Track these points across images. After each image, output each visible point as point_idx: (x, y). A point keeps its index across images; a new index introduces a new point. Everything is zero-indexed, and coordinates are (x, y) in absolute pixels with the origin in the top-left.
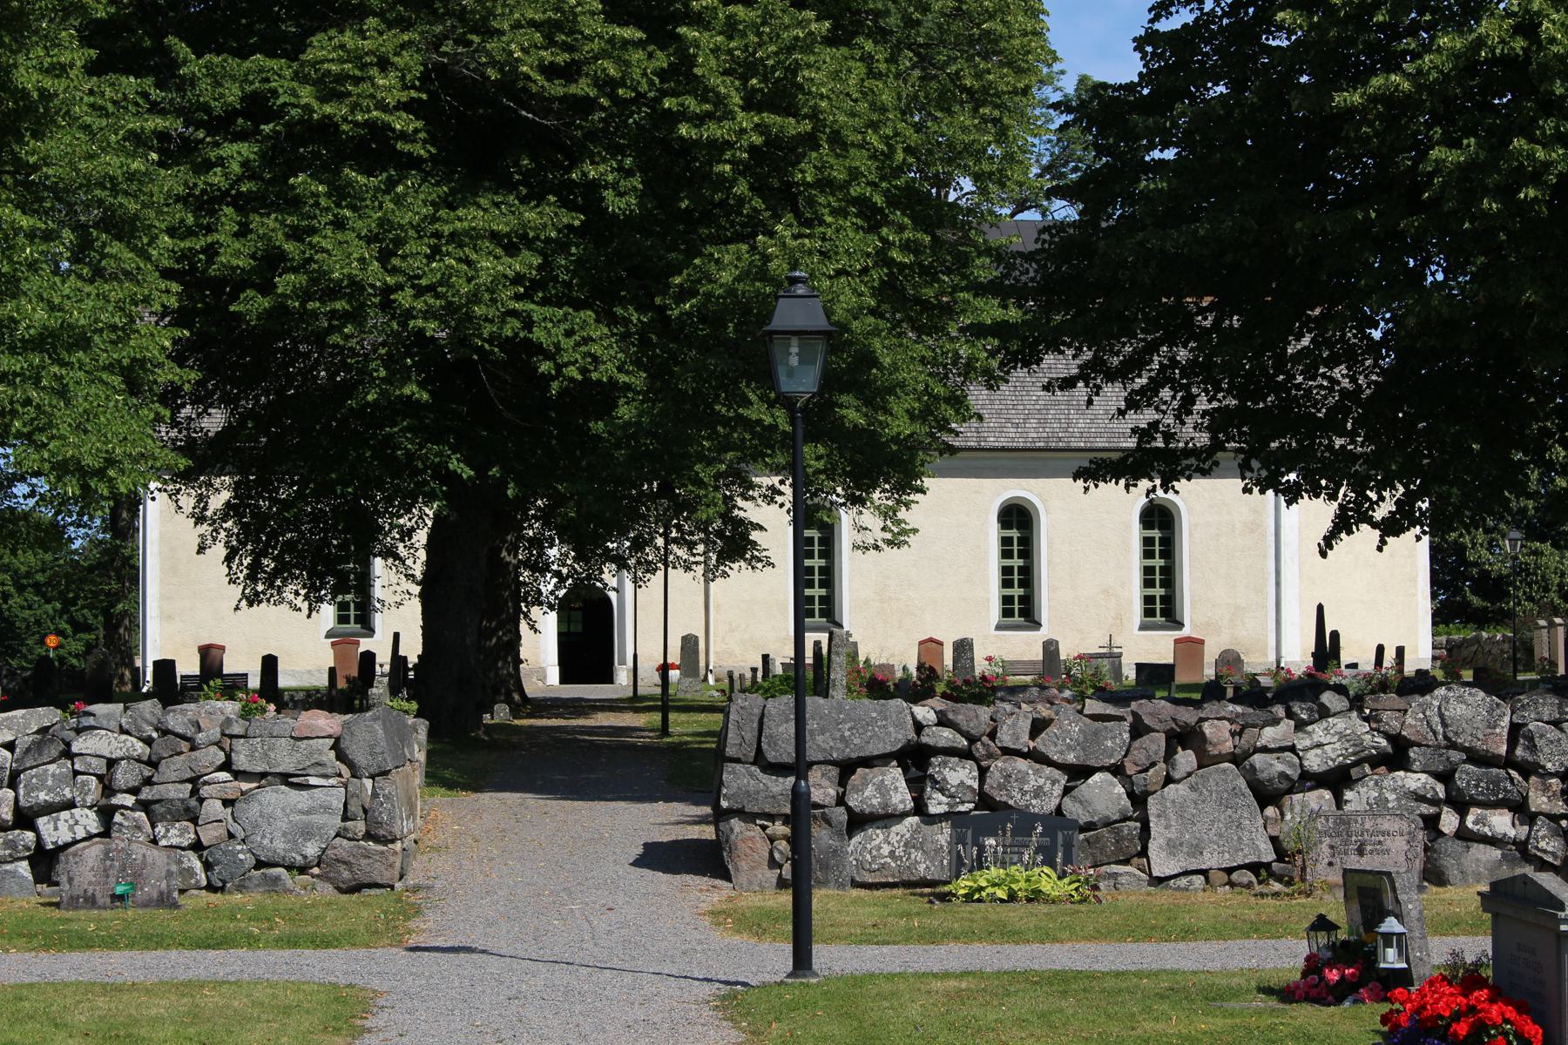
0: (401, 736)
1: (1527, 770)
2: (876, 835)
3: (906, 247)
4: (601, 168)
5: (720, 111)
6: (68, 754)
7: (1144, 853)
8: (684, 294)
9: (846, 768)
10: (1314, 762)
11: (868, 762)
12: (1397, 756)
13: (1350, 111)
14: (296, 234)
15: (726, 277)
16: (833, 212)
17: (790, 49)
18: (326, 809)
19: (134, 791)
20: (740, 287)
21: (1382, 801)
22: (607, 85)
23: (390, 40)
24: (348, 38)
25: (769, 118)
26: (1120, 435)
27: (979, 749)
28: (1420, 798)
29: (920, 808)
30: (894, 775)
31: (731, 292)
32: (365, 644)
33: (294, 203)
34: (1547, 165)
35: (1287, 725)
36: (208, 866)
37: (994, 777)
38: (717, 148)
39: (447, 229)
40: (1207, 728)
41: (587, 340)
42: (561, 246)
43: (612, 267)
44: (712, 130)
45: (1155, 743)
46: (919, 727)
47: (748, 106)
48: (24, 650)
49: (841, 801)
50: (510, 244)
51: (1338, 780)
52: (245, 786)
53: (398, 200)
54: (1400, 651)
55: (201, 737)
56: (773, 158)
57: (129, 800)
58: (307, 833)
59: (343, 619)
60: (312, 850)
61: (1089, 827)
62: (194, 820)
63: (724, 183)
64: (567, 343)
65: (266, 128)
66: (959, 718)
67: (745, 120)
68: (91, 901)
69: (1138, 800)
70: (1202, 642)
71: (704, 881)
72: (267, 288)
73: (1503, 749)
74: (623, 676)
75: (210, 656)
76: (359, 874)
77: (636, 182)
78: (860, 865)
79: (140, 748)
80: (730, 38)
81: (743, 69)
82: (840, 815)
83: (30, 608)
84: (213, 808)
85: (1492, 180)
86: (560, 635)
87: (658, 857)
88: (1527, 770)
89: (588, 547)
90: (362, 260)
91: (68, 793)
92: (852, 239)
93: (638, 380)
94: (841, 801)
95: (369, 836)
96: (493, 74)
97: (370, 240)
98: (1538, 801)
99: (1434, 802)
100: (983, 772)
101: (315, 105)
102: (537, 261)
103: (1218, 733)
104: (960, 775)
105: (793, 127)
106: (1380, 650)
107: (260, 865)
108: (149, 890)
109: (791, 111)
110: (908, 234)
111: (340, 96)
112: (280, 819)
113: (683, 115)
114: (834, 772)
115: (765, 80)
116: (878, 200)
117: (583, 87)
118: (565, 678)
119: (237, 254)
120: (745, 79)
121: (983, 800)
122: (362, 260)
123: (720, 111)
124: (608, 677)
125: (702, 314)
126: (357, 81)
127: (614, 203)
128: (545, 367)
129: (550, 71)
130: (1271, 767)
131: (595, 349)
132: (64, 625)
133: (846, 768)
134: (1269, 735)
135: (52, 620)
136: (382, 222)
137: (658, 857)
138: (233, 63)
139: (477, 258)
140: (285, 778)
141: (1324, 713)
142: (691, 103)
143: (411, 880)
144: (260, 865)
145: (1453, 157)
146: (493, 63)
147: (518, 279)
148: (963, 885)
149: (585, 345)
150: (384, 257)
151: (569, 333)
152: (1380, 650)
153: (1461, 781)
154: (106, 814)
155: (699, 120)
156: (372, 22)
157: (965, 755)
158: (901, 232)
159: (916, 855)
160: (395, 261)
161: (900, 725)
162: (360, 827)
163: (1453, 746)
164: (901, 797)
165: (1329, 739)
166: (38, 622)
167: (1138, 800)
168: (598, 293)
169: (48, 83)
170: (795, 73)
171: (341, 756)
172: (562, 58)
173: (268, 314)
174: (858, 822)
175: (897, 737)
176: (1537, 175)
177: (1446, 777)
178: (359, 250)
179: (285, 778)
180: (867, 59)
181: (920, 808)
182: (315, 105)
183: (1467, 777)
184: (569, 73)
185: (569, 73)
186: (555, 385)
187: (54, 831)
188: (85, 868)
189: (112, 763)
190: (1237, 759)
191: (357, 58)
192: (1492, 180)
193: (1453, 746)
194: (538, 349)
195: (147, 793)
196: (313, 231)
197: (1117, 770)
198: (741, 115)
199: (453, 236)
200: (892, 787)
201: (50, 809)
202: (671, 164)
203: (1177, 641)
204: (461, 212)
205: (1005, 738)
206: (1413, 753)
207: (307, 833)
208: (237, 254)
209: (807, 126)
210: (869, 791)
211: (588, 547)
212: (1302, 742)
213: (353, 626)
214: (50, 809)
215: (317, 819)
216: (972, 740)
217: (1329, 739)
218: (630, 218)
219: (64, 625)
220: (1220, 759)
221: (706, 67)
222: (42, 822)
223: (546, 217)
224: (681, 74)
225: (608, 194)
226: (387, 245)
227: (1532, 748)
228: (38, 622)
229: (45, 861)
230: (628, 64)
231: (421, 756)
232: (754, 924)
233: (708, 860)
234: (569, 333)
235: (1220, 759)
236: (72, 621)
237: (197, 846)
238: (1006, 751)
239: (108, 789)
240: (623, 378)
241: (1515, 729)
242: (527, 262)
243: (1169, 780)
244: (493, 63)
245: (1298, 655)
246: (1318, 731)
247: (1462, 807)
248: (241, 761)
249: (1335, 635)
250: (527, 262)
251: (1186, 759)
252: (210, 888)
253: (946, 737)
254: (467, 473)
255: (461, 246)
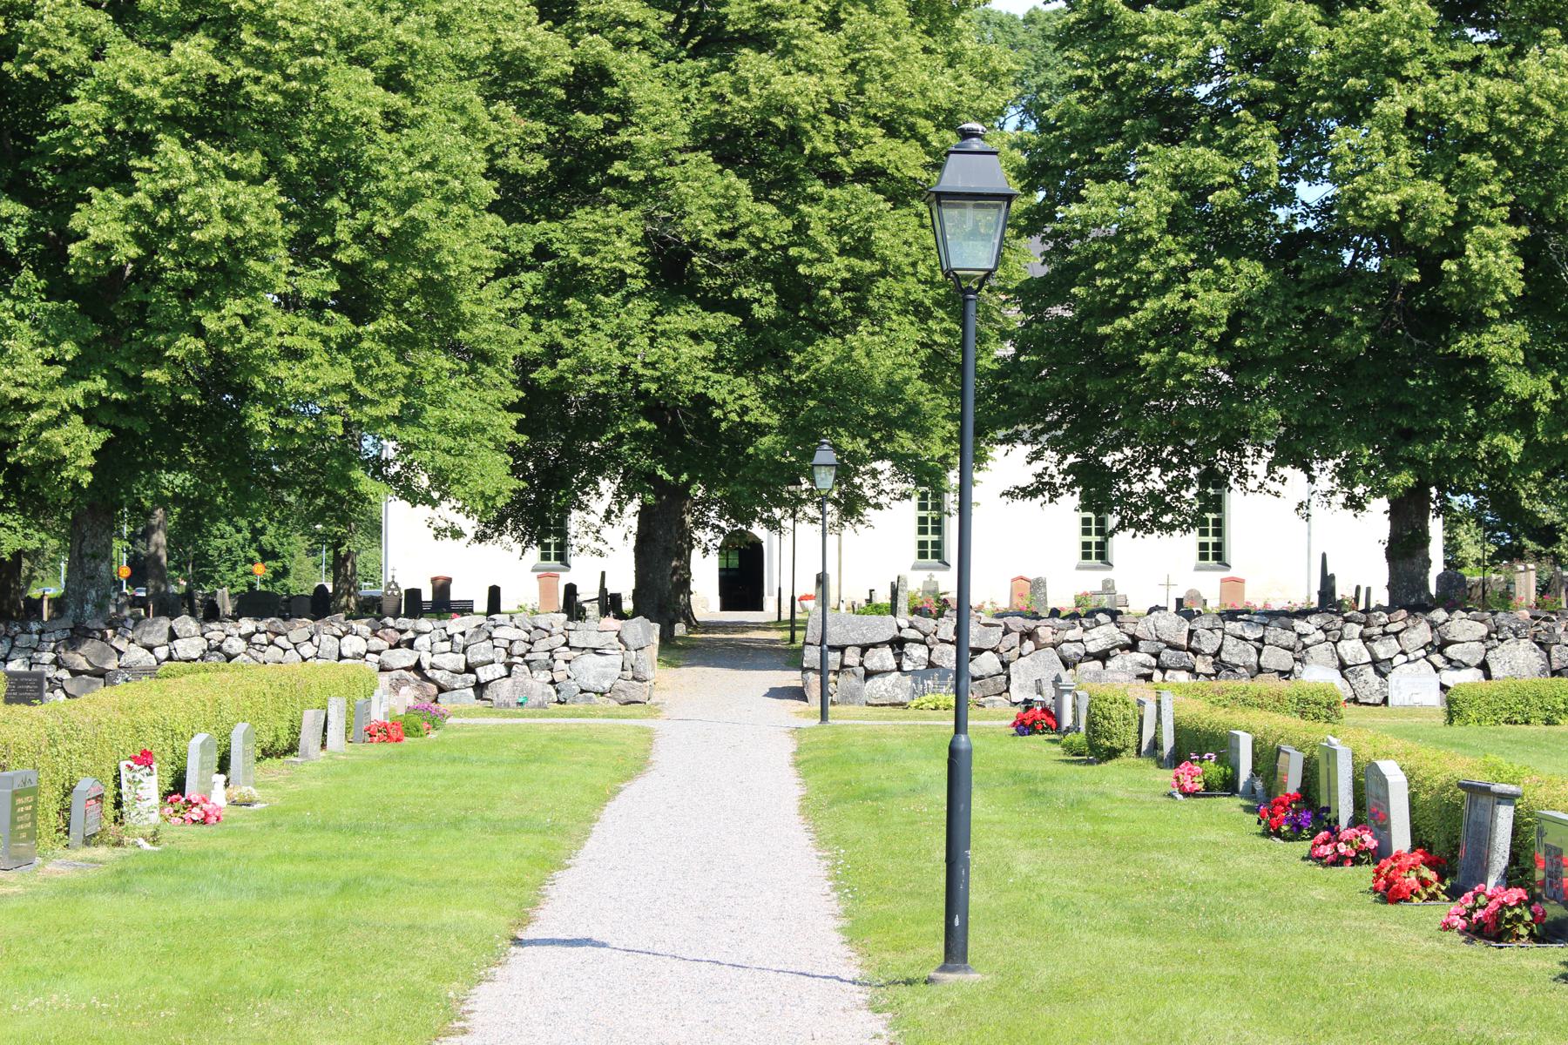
0: (648, 632)
1: (1196, 652)
2: (877, 680)
3: (947, 332)
4: (751, 290)
5: (824, 257)
6: (490, 638)
7: (1007, 690)
8: (800, 369)
9: (864, 649)
10: (1092, 648)
11: (874, 646)
12: (1133, 645)
13: (1107, 337)
14: (569, 334)
15: (827, 360)
16: (898, 313)
17: (867, 220)
18: (614, 665)
19: (522, 656)
20: (838, 367)
21: (1124, 667)
22: (755, 242)
23: (623, 218)
24: (598, 216)
25: (854, 261)
26: (1026, 478)
27: (929, 640)
28: (1144, 666)
29: (899, 668)
30: (887, 652)
31: (831, 370)
32: (565, 578)
33: (565, 315)
34: (1195, 365)
35: (1079, 629)
36: (558, 691)
37: (935, 654)
38: (822, 281)
39: (659, 328)
40: (1039, 630)
41: (742, 397)
42: (729, 335)
43: (759, 351)
44: (820, 270)
45: (1014, 638)
46: (900, 629)
47: (842, 252)
48: (217, 576)
49: (861, 664)
50: (695, 337)
51: (1103, 656)
52: (575, 653)
53: (629, 313)
54: (1368, 590)
55: (554, 631)
56: (857, 286)
57: (520, 660)
58: (605, 676)
59: (545, 557)
60: (607, 685)
61: (981, 678)
62: (551, 670)
63: (826, 302)
64: (730, 399)
65: (547, 264)
66: (919, 625)
67: (840, 262)
68: (507, 705)
69: (1005, 665)
70: (1242, 581)
71: (796, 702)
72: (553, 365)
73: (1184, 642)
74: (770, 602)
75: (442, 587)
76: (628, 696)
77: (773, 298)
78: (870, 695)
79: (526, 636)
80: (831, 210)
81: (836, 230)
82: (861, 671)
83: (222, 537)
84: (560, 664)
85: (1171, 370)
86: (721, 570)
87: (776, 693)
88: (1196, 652)
89: (739, 510)
90: (609, 350)
91: (491, 657)
92: (908, 331)
93: (774, 420)
94: (861, 664)
95: (634, 678)
96: (686, 238)
97: (614, 337)
98: (1200, 668)
99: (1150, 667)
100: (930, 651)
101: (579, 257)
102: (715, 347)
103: (1045, 633)
104: (918, 652)
105: (868, 267)
106: (1358, 588)
107: (582, 691)
108: (534, 701)
109: (871, 256)
110: (945, 325)
111: (592, 253)
112: (591, 670)
113: (800, 260)
114: (858, 650)
115: (852, 236)
116: (928, 302)
117: (740, 243)
118: (726, 606)
119: (534, 344)
120: (840, 237)
121: (931, 665)
122: (609, 350)
123: (824, 257)
124: (758, 605)
125: (813, 379)
126: (605, 244)
127: (758, 312)
128: (717, 413)
129: (722, 235)
130: (1070, 650)
131: (746, 402)
132: (252, 553)
133: (864, 649)
134: (1070, 635)
135: (243, 548)
136: (619, 326)
137: (776, 693)
138: (528, 227)
139: (680, 349)
140: (594, 650)
141: (1098, 624)
142: (807, 253)
143: (653, 700)
144: (582, 691)
145: (1154, 359)
146: (686, 232)
147: (704, 359)
148: (916, 702)
149: (739, 397)
150: (621, 347)
151: (731, 392)
152: (1358, 588)
153: (1163, 657)
154: (509, 666)
155: (810, 263)
156: (613, 206)
157: (923, 643)
158: (942, 322)
159: (898, 690)
160: (628, 349)
161: (890, 628)
162: (629, 674)
163: (1160, 640)
164: (891, 663)
165: (1102, 635)
166: (229, 550)
167: (1005, 665)
168: (747, 365)
169: (476, 309)
170: (870, 234)
171: (621, 641)
172: (727, 227)
173: (553, 382)
174: (869, 674)
175: (889, 633)
176: (1191, 369)
177: (1156, 656)
178: (606, 343)
179: (594, 650)
180: (920, 215)
181: (899, 668)
182: (579, 257)
183: (1167, 655)
184: (731, 235)
185: (731, 235)
186: (724, 425)
187: (484, 674)
188: (503, 691)
189: (511, 642)
190: (1054, 646)
191: (605, 229)
192: (1171, 370)
193: (1160, 640)
194: (712, 402)
195: (528, 657)
196: (578, 332)
197: (995, 650)
198: (836, 259)
199: (663, 333)
200: (883, 658)
201: (483, 664)
202: (795, 290)
203: (1223, 581)
204: (667, 318)
205: (941, 635)
206: (1141, 643)
207: (605, 676)
208: (534, 344)
209: (877, 267)
210: (875, 659)
211: (739, 510)
212: (1086, 637)
213: (553, 563)
214: (483, 664)
215: (610, 670)
216: (926, 636)
217: (1102, 635)
218: (769, 321)
219: (252, 553)
220: (1045, 646)
221: (817, 231)
222: (479, 670)
223: (720, 321)
224: (801, 228)
225: (755, 306)
226: (621, 339)
227: (1199, 641)
228: (229, 550)
229: (480, 688)
230: (768, 229)
231: (657, 642)
232: (808, 715)
233: (799, 694)
234: (731, 392)
235: (1045, 646)
236: (261, 550)
237: (553, 682)
238: (942, 641)
239: (510, 655)
240: (765, 420)
241: (1191, 633)
242: (708, 348)
243: (1021, 655)
244: (686, 232)
245: (1305, 592)
246: (1094, 633)
247: (1163, 670)
248: (573, 643)
249: (1333, 577)
250: (708, 348)
251: (1029, 645)
252: (559, 702)
253: (912, 634)
254: (666, 476)
255: (669, 338)
